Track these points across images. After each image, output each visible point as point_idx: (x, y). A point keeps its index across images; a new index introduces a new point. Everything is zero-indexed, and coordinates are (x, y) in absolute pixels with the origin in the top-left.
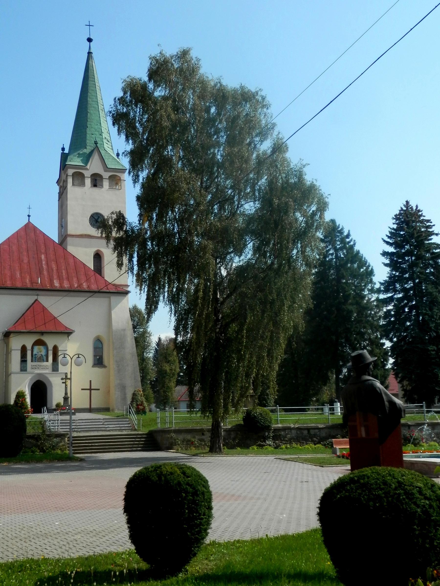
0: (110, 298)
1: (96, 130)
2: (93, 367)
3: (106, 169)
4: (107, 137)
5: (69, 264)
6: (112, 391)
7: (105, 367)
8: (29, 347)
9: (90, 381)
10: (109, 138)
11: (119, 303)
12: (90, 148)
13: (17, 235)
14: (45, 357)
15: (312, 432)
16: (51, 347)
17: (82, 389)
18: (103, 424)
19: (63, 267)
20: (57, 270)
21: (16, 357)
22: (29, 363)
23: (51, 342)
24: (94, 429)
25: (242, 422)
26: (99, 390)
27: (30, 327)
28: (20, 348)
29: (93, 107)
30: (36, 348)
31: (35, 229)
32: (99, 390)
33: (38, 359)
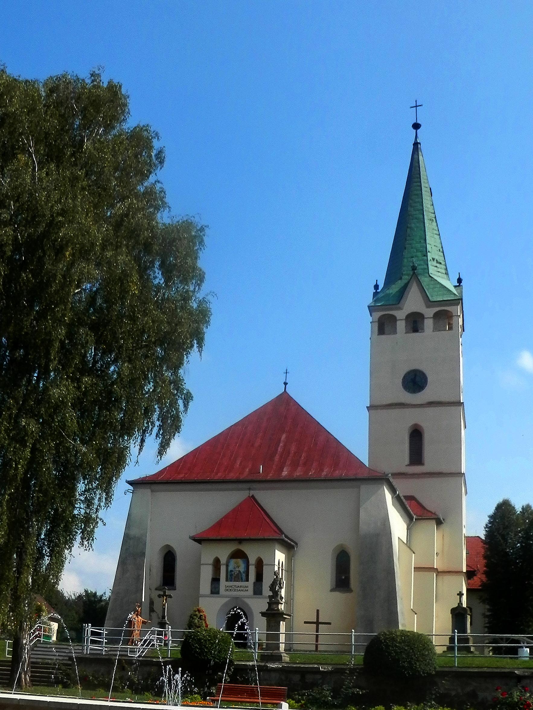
1: (417, 251)
2: (332, 590)
3: (429, 303)
4: (436, 257)
9: (318, 611)
10: (441, 259)
12: (406, 277)
14: (244, 576)
15: (309, 678)
16: (252, 560)
17: (305, 622)
21: (207, 574)
22: (223, 583)
23: (253, 553)
25: (179, 656)
28: (211, 561)
30: (233, 561)
32: (329, 624)
33: (235, 577)
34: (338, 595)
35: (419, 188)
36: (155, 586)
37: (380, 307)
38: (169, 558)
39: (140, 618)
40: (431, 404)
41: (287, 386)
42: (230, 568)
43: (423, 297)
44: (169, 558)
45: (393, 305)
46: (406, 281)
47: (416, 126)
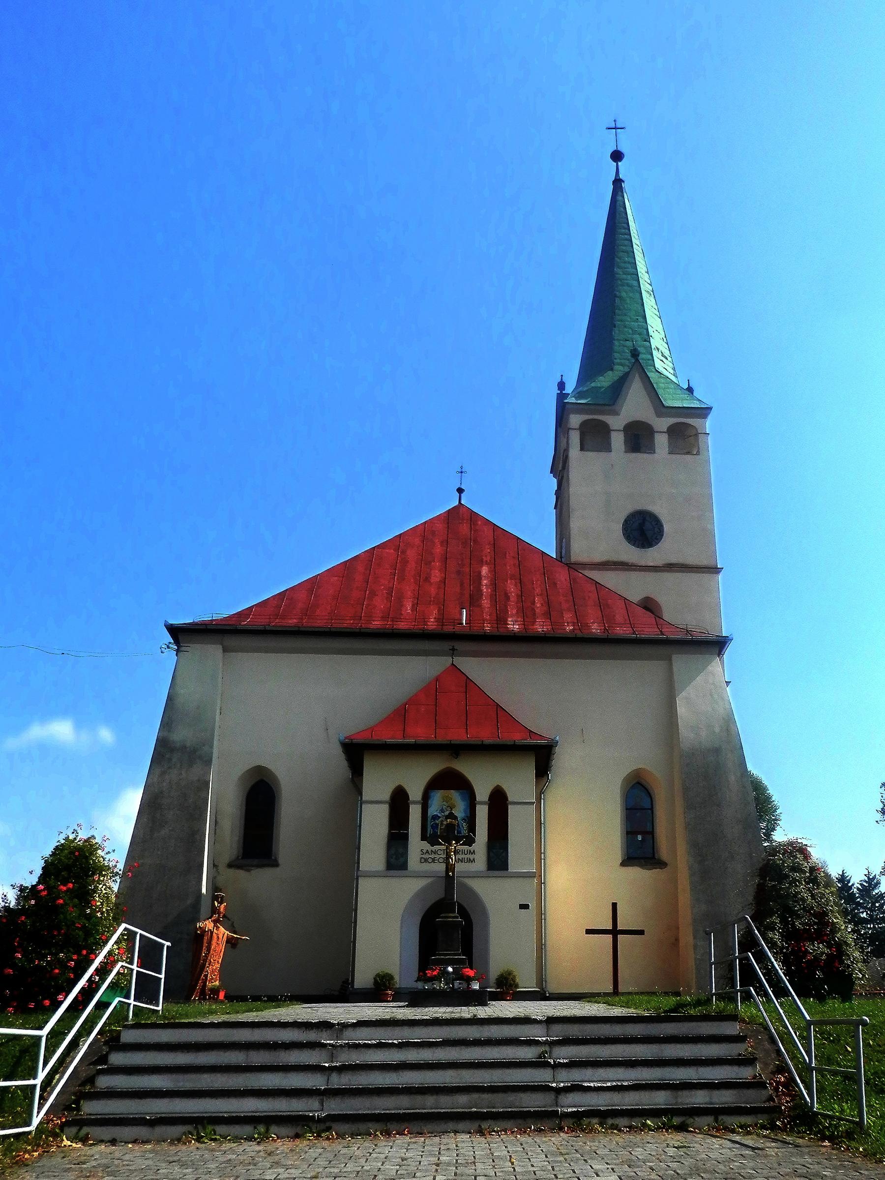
0: (670, 659)
1: (634, 332)
2: (624, 864)
5: (555, 584)
6: (687, 938)
7: (661, 864)
8: (415, 793)
9: (614, 905)
11: (699, 672)
12: (621, 368)
13: (425, 531)
16: (482, 793)
17: (589, 932)
18: (539, 1064)
19: (538, 591)
20: (520, 596)
21: (375, 823)
22: (416, 844)
23: (483, 778)
24: (461, 1103)
26: (641, 932)
27: (420, 733)
28: (386, 795)
29: (628, 285)
31: (473, 516)
32: (641, 932)
34: (635, 872)
35: (626, 242)
36: (226, 858)
37: (581, 406)
38: (260, 796)
39: (222, 929)
40: (670, 567)
41: (462, 495)
42: (433, 810)
43: (650, 397)
44: (260, 796)
45: (604, 405)
46: (620, 374)
47: (617, 156)
